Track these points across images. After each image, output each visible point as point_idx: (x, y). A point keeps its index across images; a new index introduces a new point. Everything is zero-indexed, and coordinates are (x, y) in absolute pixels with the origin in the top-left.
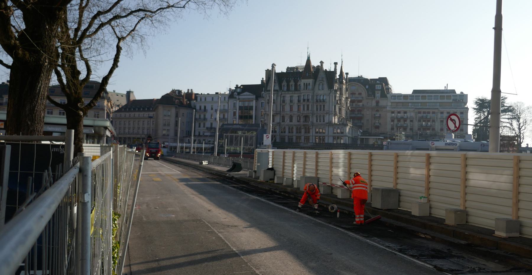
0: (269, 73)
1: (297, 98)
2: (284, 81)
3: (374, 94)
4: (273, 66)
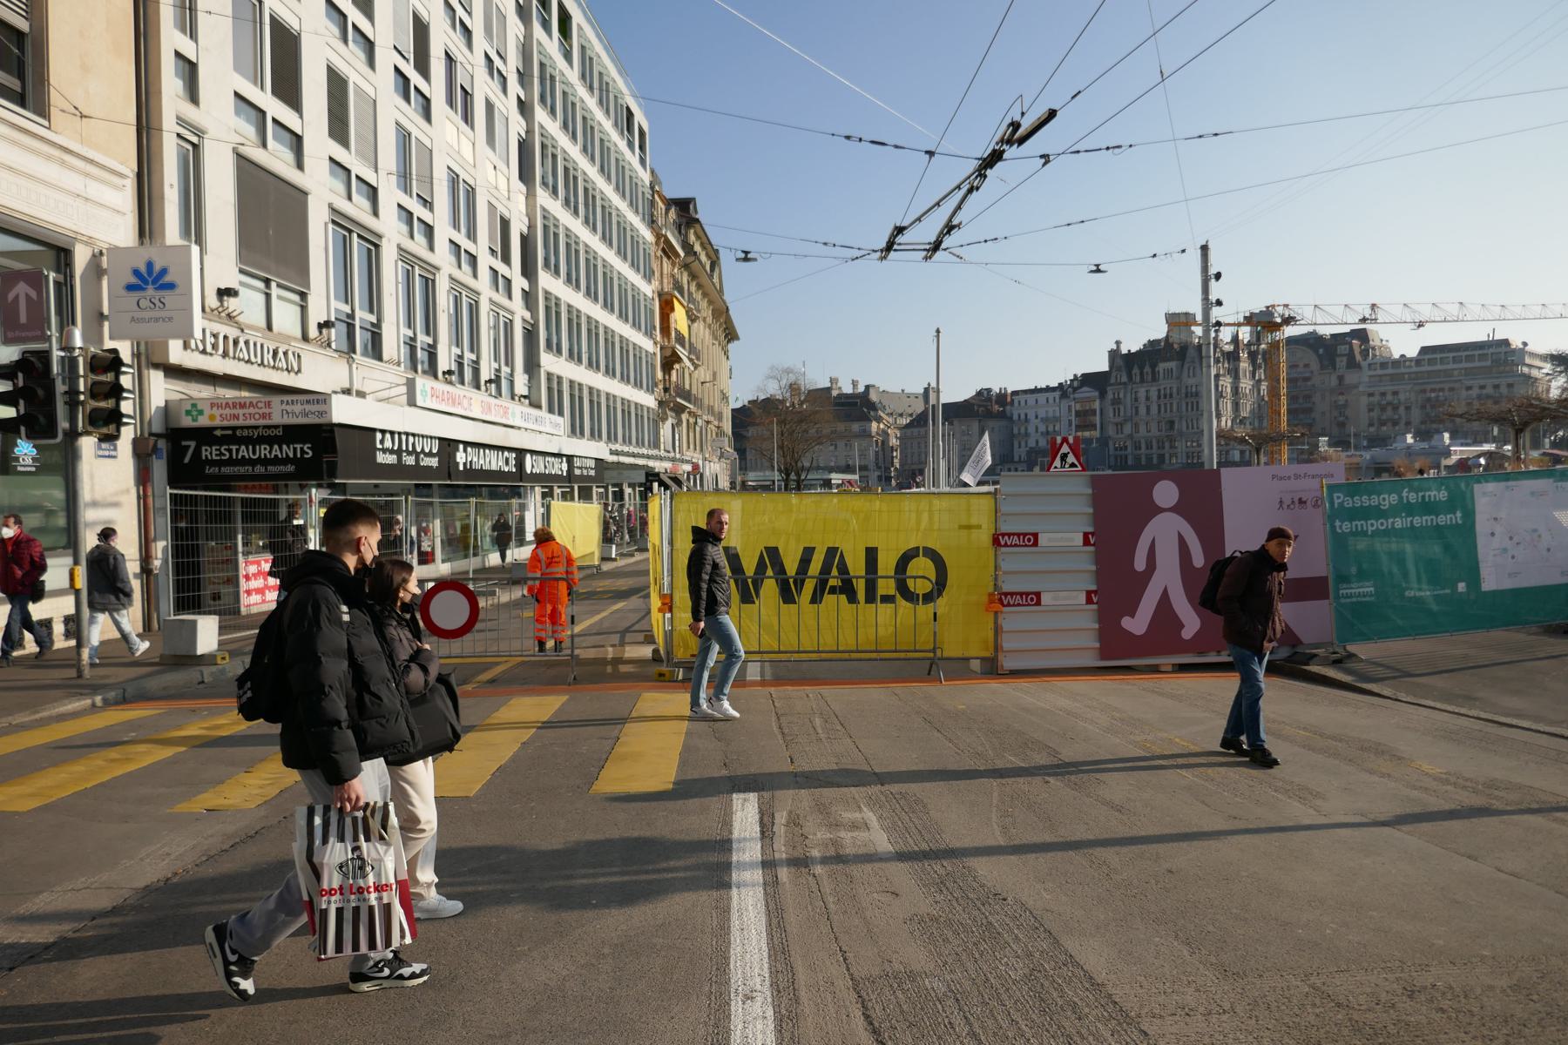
0: (1114, 355)
1: (1157, 393)
2: (1136, 366)
4: (1118, 343)
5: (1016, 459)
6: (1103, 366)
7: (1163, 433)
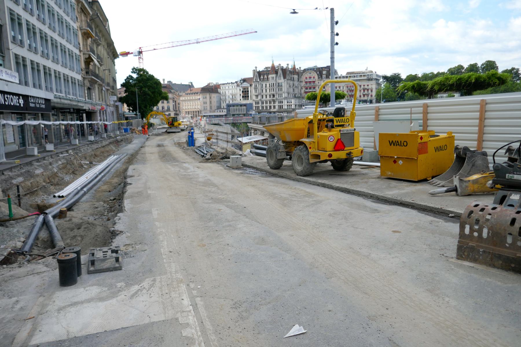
4: (256, 67)
5: (222, 107)
6: (251, 76)
7: (271, 99)
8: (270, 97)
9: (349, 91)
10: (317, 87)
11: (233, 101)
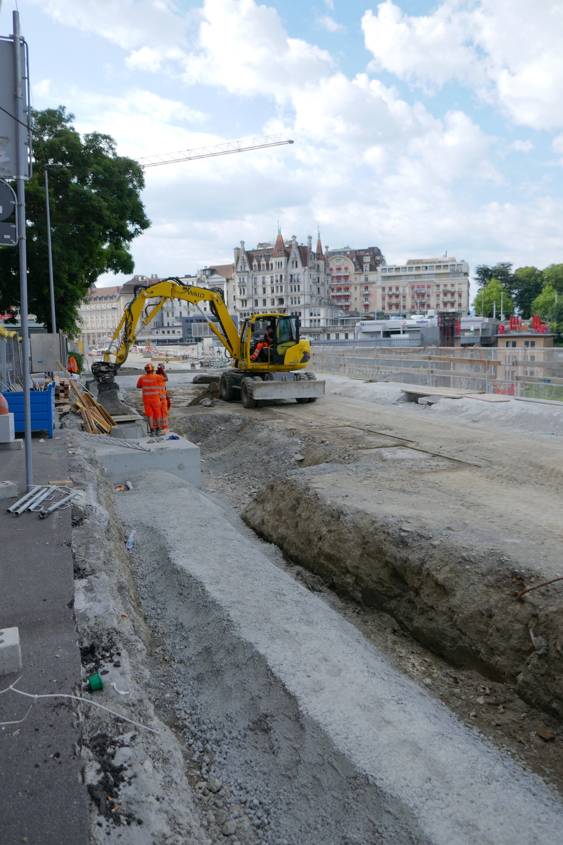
1: (270, 279)
3: (362, 268)
5: (166, 324)
6: (230, 260)
8: (273, 304)
9: (416, 296)
10: (353, 287)
11: (189, 313)
